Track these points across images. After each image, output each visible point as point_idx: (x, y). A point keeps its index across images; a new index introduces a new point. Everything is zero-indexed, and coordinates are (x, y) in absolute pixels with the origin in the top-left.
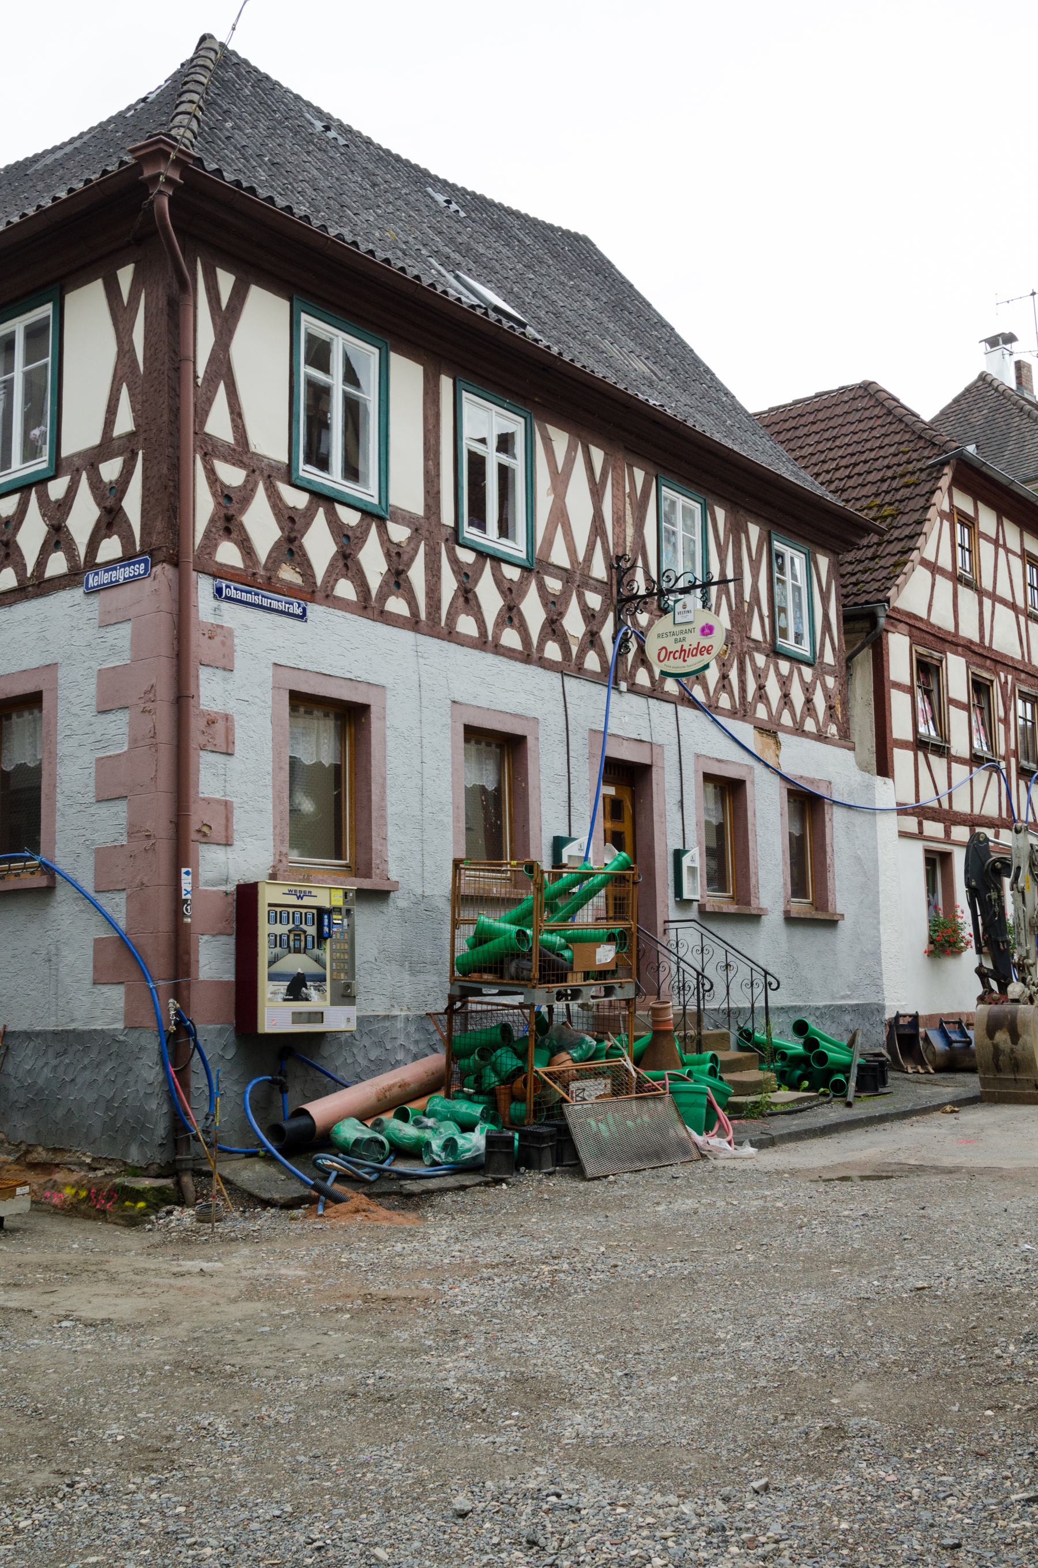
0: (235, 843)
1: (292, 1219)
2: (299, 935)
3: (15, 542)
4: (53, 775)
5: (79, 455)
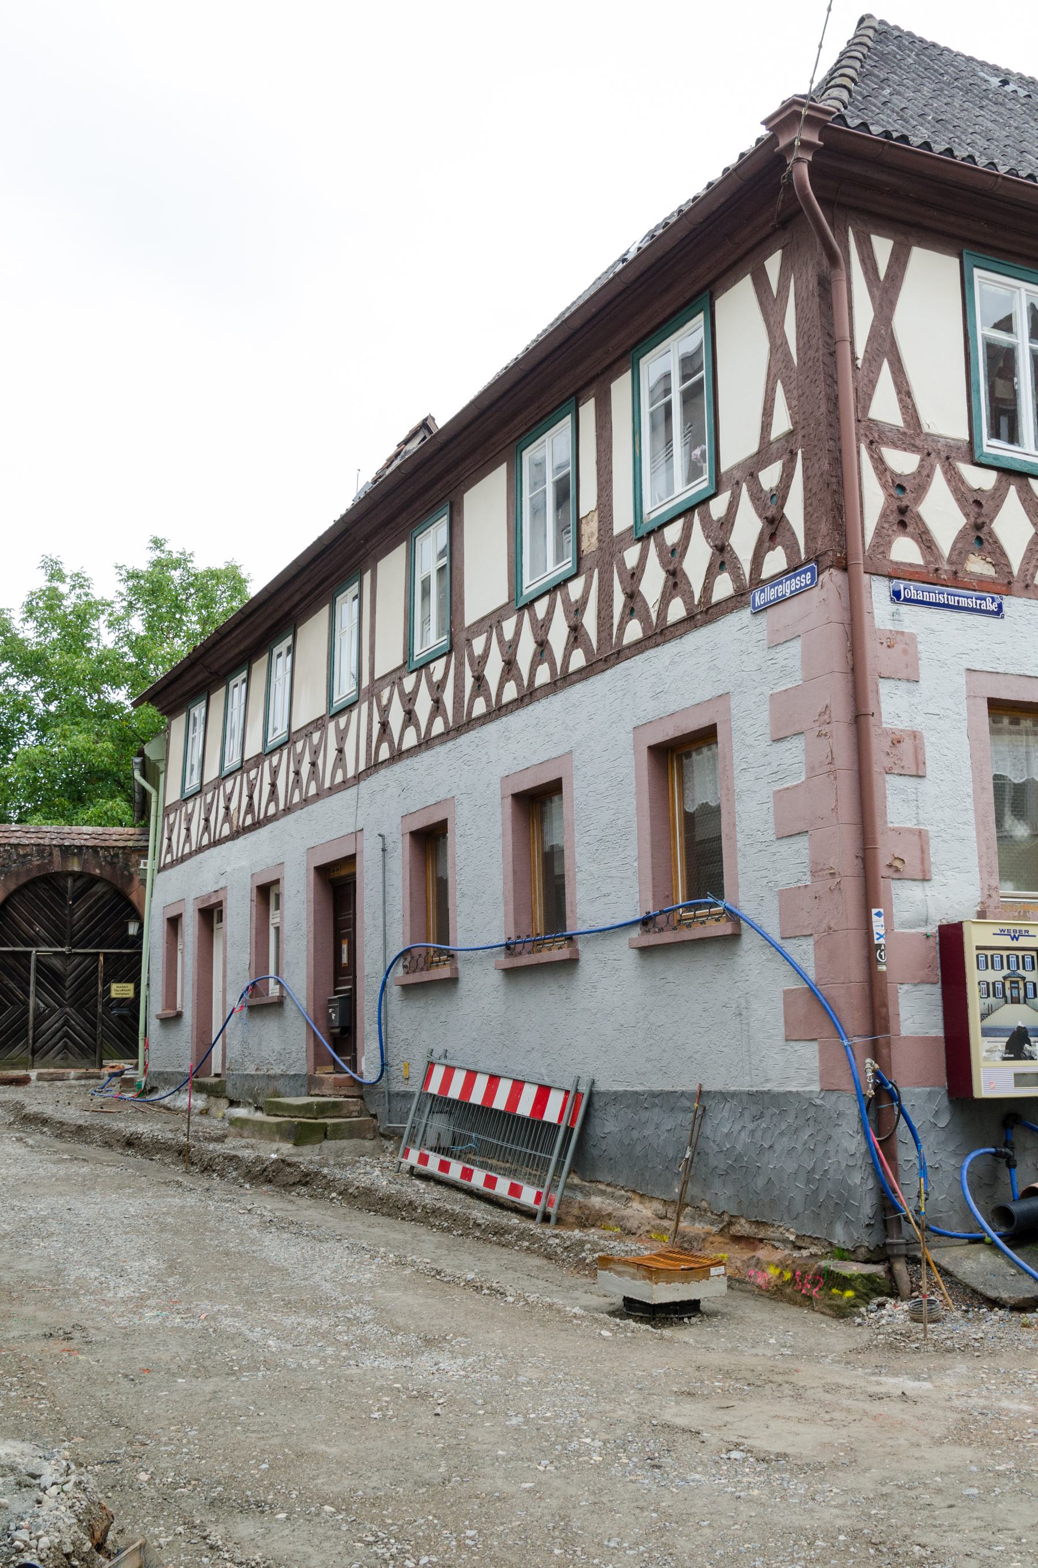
0: (934, 877)
1: (1024, 1326)
2: (1017, 982)
3: (682, 569)
4: (732, 813)
5: (738, 466)
